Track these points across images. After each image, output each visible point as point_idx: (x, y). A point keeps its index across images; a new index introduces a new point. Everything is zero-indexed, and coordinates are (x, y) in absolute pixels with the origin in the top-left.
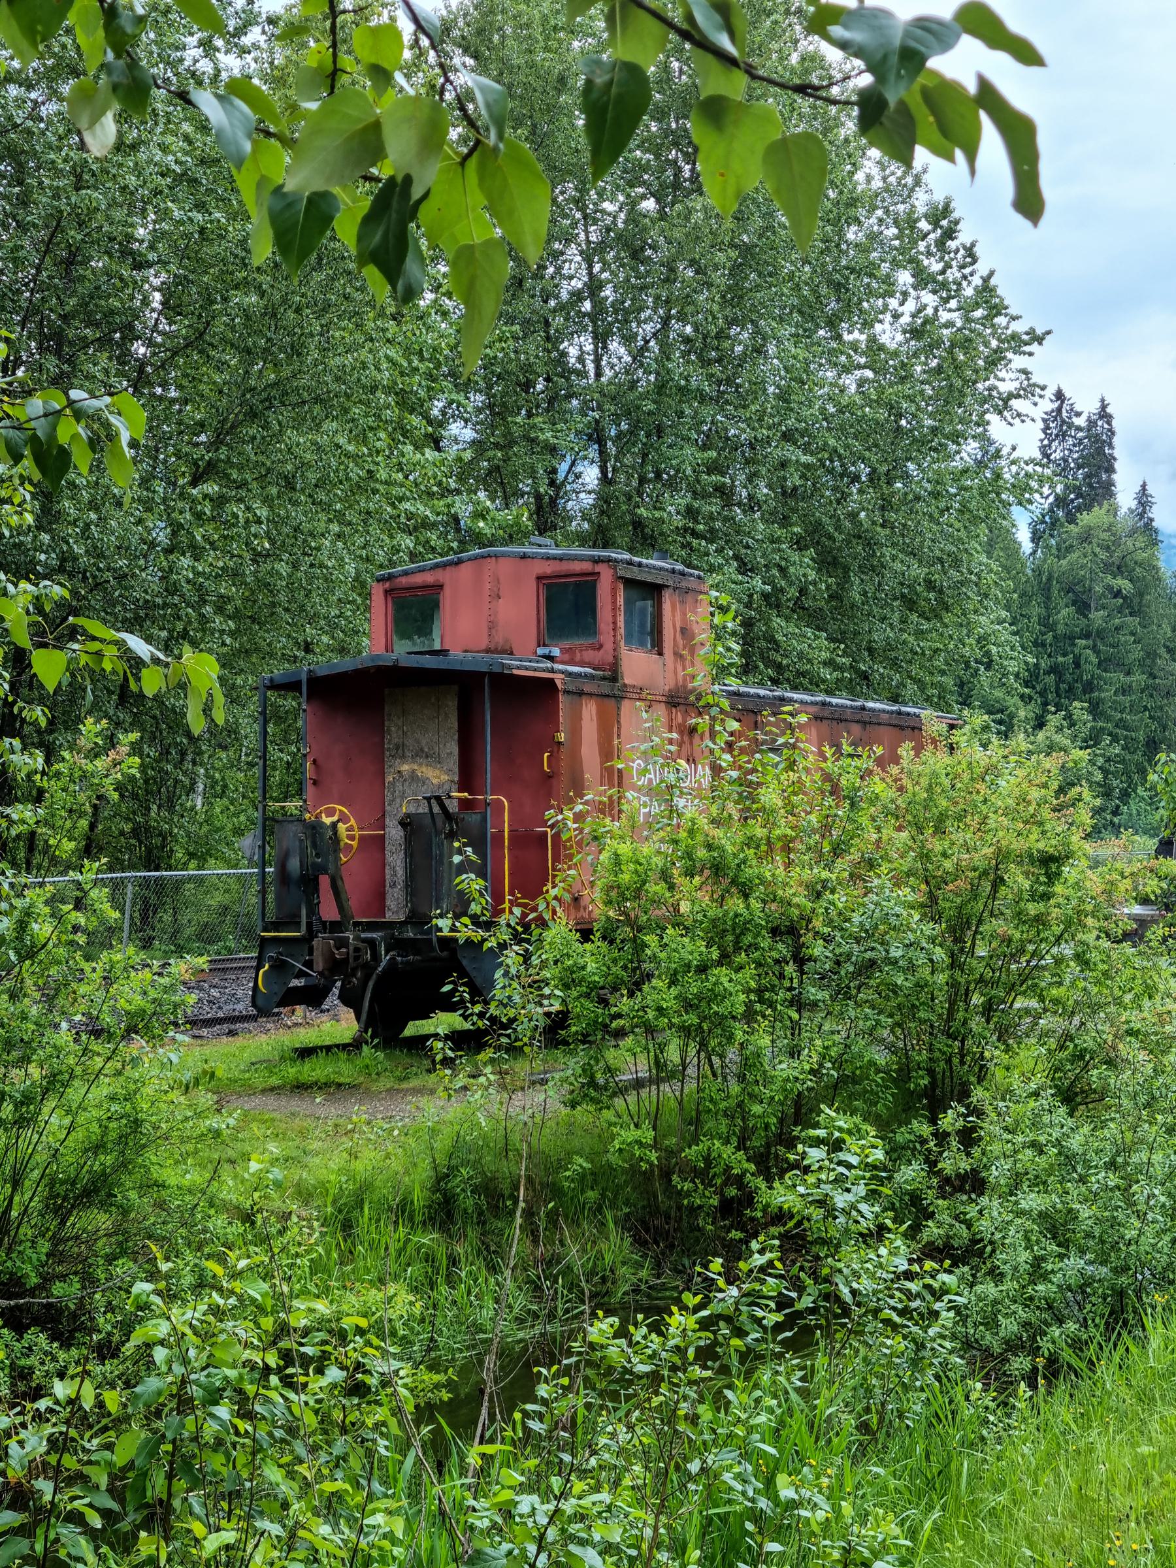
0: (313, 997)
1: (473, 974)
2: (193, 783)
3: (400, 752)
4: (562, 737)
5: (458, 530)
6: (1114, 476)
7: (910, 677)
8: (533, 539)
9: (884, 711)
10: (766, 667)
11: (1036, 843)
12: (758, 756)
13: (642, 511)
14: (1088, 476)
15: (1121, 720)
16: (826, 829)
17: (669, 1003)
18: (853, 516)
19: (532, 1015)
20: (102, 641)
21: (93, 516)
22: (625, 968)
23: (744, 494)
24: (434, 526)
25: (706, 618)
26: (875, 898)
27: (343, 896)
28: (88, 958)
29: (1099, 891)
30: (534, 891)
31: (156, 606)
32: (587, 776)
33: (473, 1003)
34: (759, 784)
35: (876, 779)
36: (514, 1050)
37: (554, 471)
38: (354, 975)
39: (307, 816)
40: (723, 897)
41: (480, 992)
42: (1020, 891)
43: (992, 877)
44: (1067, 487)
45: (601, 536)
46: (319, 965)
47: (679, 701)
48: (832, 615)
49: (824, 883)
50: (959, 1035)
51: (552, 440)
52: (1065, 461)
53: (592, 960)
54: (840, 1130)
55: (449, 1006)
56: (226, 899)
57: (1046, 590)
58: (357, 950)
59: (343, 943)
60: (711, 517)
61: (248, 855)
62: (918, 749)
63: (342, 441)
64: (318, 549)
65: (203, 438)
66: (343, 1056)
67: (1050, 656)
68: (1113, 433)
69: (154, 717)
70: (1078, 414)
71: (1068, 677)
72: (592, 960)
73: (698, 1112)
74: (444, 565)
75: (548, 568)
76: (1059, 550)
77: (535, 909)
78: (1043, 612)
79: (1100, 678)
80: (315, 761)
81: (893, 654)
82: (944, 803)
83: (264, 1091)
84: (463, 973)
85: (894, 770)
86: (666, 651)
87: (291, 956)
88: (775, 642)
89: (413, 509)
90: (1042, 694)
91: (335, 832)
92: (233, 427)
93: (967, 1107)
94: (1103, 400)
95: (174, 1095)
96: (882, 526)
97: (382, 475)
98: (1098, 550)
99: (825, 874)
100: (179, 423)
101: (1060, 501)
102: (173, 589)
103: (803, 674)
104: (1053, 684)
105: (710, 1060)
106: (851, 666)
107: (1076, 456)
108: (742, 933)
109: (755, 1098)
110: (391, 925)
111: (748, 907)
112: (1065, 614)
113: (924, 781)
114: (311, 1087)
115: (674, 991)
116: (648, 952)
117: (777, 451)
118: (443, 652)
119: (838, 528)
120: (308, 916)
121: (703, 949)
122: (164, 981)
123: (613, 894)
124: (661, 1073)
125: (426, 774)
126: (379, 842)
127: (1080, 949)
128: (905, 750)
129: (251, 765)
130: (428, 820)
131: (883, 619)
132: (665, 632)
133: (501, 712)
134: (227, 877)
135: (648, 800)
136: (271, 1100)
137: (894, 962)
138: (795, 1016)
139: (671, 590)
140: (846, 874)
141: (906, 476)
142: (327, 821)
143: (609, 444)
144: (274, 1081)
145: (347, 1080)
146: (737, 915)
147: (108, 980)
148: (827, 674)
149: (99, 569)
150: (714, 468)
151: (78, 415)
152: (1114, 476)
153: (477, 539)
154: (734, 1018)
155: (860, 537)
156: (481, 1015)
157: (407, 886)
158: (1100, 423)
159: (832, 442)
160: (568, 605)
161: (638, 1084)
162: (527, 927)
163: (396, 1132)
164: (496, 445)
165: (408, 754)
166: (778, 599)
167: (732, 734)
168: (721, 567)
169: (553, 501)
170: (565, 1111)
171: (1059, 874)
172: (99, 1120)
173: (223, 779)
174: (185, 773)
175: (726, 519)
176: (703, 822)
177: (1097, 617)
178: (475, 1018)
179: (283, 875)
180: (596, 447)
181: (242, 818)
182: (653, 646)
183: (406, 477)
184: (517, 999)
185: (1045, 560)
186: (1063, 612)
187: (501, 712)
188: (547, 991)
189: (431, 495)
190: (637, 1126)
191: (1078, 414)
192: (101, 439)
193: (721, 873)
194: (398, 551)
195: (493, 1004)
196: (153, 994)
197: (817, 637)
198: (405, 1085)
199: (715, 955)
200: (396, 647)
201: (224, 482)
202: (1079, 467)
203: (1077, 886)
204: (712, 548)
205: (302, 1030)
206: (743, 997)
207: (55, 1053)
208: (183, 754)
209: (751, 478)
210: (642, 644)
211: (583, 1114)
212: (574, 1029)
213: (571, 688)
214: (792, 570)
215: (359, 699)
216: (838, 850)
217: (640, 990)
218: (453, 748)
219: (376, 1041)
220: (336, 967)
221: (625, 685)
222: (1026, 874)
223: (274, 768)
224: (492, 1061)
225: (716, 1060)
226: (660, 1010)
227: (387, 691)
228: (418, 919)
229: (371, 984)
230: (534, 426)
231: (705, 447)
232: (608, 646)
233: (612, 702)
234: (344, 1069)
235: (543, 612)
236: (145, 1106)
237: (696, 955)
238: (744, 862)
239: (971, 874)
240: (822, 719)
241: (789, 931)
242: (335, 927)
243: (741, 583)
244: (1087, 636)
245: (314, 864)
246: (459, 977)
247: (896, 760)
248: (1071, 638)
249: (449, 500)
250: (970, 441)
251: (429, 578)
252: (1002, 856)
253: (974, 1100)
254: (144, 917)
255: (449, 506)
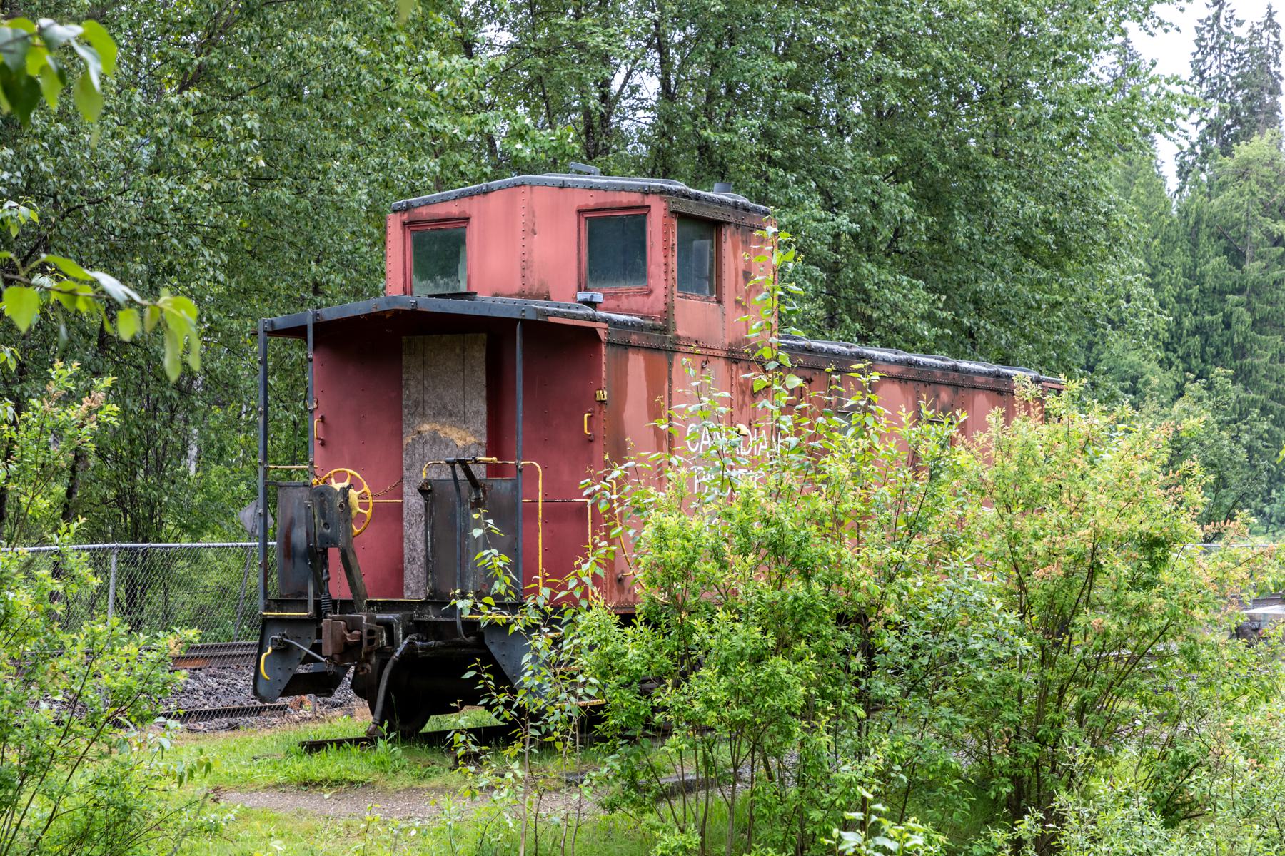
0: (322, 685)
1: (502, 661)
2: (186, 445)
3: (420, 410)
4: (603, 395)
5: (493, 152)
6: (1279, 99)
7: (1024, 336)
8: (574, 165)
9: (979, 373)
10: (853, 321)
11: (1139, 523)
12: (820, 419)
13: (707, 133)
14: (1249, 98)
15: (1277, 391)
16: (901, 503)
17: (718, 695)
18: (960, 142)
19: (564, 707)
20: (76, 280)
21: (62, 128)
22: (670, 655)
23: (832, 114)
24: (463, 146)
25: (764, 263)
26: (952, 582)
27: (355, 572)
28: (66, 628)
29: (1209, 579)
30: (560, 566)
31: (135, 236)
32: (628, 439)
33: (499, 692)
34: (825, 452)
35: (959, 448)
36: (546, 748)
37: (606, 83)
38: (368, 661)
39: (315, 480)
40: (781, 578)
41: (505, 680)
42: (1118, 578)
43: (1088, 562)
44: (1222, 110)
45: (662, 164)
46: (328, 649)
47: (736, 357)
48: (931, 261)
49: (898, 565)
50: (1048, 740)
51: (603, 47)
52: (1222, 80)
53: (634, 648)
54: (878, 813)
55: (472, 699)
56: (223, 579)
57: (1193, 235)
58: (371, 632)
59: (353, 625)
60: (792, 141)
61: (249, 528)
62: (1008, 417)
63: (351, 42)
64: (325, 172)
65: (193, 38)
66: (356, 750)
67: (1195, 314)
68: (1280, 47)
69: (139, 367)
70: (1239, 23)
71: (1216, 339)
72: (634, 648)
73: (752, 818)
74: (471, 195)
75: (591, 200)
76: (1210, 186)
77: (564, 587)
78: (1189, 261)
79: (1254, 341)
80: (322, 418)
81: (1004, 308)
82: (1037, 478)
83: (267, 788)
84: (488, 658)
85: (981, 438)
86: (726, 298)
87: (298, 639)
88: (865, 292)
89: (439, 127)
90: (1185, 358)
91: (346, 500)
92: (225, 26)
93: (1047, 813)
94: (1270, 7)
95: (167, 782)
96: (995, 155)
97: (403, 84)
98: (1256, 188)
99: (897, 555)
100: (165, 20)
101: (1214, 127)
102: (152, 215)
103: (897, 330)
104: (1198, 347)
105: (766, 762)
106: (955, 322)
107: (1234, 73)
108: (802, 619)
109: (814, 803)
110: (409, 605)
111: (809, 589)
112: (1214, 264)
113: (1016, 453)
114: (319, 784)
115: (724, 682)
116: (696, 638)
117: (871, 60)
118: (470, 295)
119: (943, 158)
120: (316, 595)
121: (758, 635)
122: (153, 656)
123: (659, 574)
124: (712, 777)
125: (450, 435)
126: (397, 512)
127: (1187, 646)
128: (994, 417)
129: (251, 424)
130: (452, 487)
131: (993, 266)
132: (725, 276)
133: (537, 367)
134: (224, 558)
135: (707, 473)
136: (275, 798)
137: (973, 655)
138: (862, 713)
139: (733, 228)
140: (925, 557)
141: (1026, 97)
142: (337, 486)
143: (672, 51)
144: (279, 777)
145: (361, 778)
146: (796, 599)
147: (91, 654)
148: (923, 328)
149: (71, 192)
150: (795, 82)
151: (49, 44)
152: (1279, 99)
153: (517, 165)
154: (793, 714)
155: (968, 168)
156: (508, 705)
157: (428, 562)
158: (1265, 34)
159: (935, 52)
160: (612, 241)
161: (687, 788)
162: (557, 609)
163: (414, 832)
164: (538, 51)
165: (429, 412)
166: (869, 240)
167: (792, 392)
168: (801, 200)
169: (605, 119)
170: (603, 815)
171: (1165, 560)
172: (84, 807)
173: (220, 441)
174: (175, 433)
175: (808, 145)
176: (759, 494)
177: (1253, 268)
178: (501, 708)
179: (288, 550)
180: (657, 55)
181: (243, 487)
182: (711, 293)
183: (432, 88)
184: (548, 688)
185: (1193, 200)
186: (1214, 262)
187: (537, 367)
188: (581, 678)
189: (460, 109)
190: (682, 831)
191: (1239, 23)
192: (68, 70)
193: (782, 553)
194: (421, 175)
195: (521, 693)
196: (140, 670)
197: (913, 287)
198: (425, 784)
199: (771, 643)
200: (416, 289)
201: (217, 91)
202: (1238, 87)
203: (1184, 575)
204: (791, 178)
205: (311, 725)
206: (801, 690)
207: (34, 733)
208: (173, 412)
209: (841, 93)
210: (700, 290)
211: (623, 818)
212: (612, 722)
213: (615, 339)
214: (886, 206)
215: (376, 348)
216: (915, 527)
217: (687, 681)
218: (480, 406)
219: (393, 735)
220: (348, 651)
221: (678, 337)
222: (1127, 560)
223: (280, 429)
224: (520, 755)
225: (773, 761)
226: (709, 703)
227: (405, 339)
228: (438, 599)
229: (387, 672)
230: (582, 29)
231: (786, 57)
232: (660, 291)
233: (661, 358)
234: (354, 765)
235: (585, 250)
236: (135, 794)
237: (750, 642)
238: (806, 540)
239: (1063, 559)
240: (907, 380)
241: (855, 619)
242: (346, 606)
243: (825, 220)
244: (1240, 291)
245: (322, 535)
246: (483, 663)
247: (984, 427)
248: (1221, 293)
249: (482, 116)
250: (1103, 53)
251: (453, 209)
252: (1100, 537)
253: (1057, 805)
254: (131, 599)
255: (483, 123)
